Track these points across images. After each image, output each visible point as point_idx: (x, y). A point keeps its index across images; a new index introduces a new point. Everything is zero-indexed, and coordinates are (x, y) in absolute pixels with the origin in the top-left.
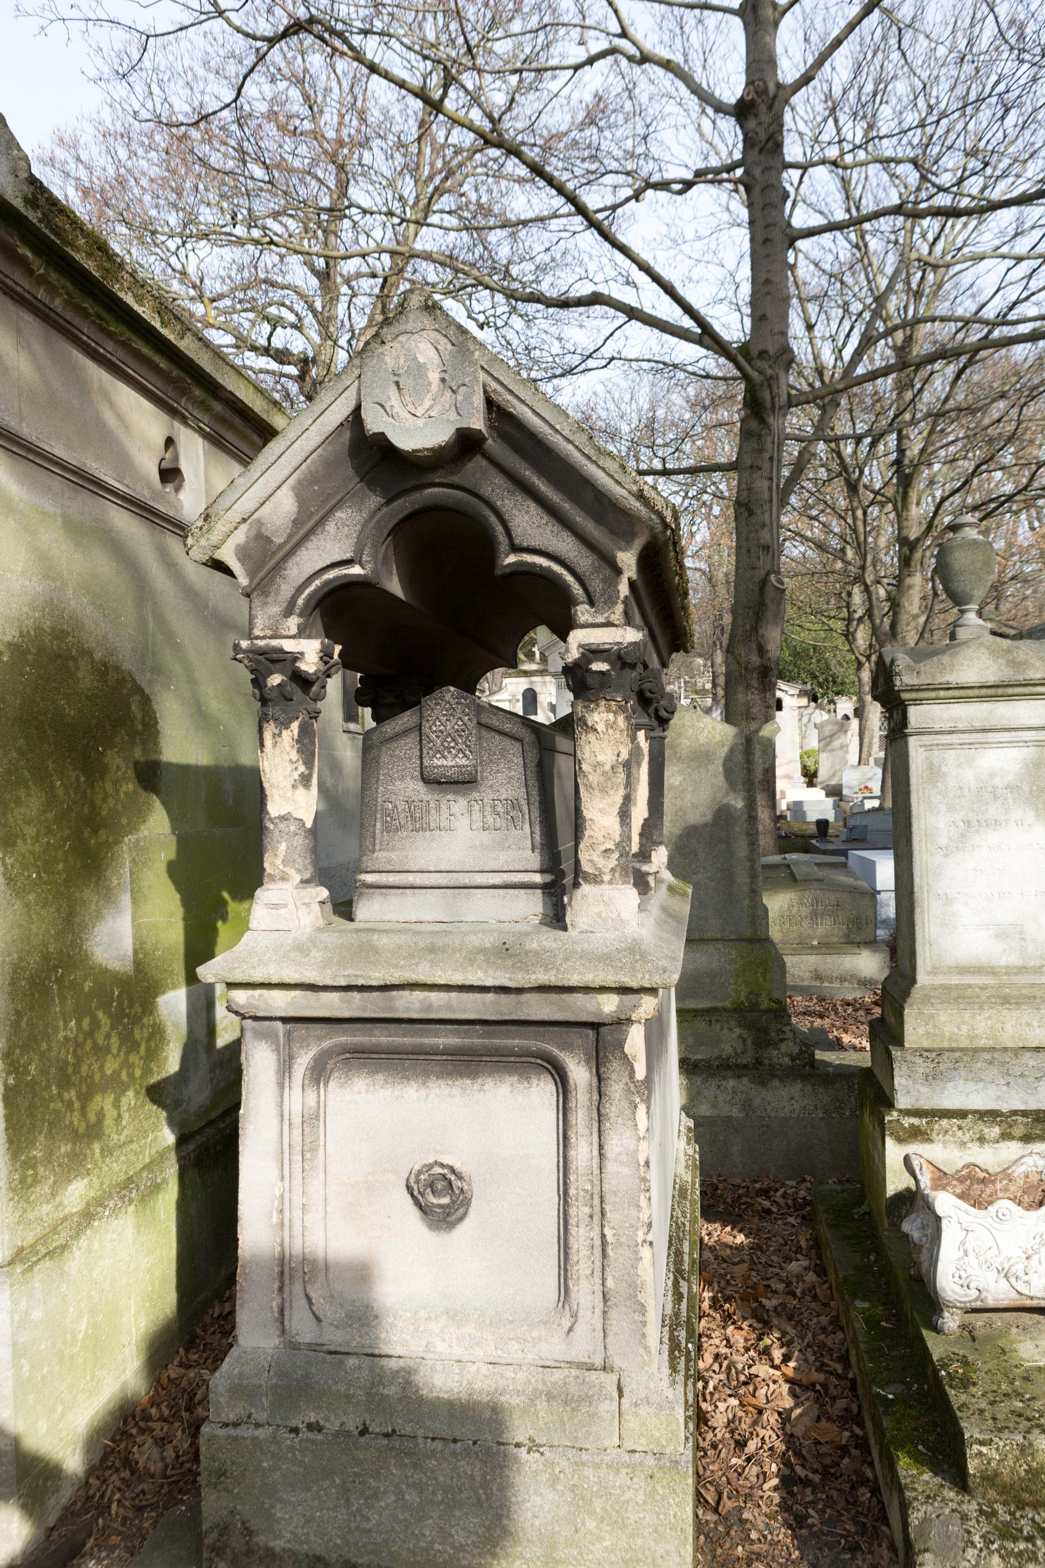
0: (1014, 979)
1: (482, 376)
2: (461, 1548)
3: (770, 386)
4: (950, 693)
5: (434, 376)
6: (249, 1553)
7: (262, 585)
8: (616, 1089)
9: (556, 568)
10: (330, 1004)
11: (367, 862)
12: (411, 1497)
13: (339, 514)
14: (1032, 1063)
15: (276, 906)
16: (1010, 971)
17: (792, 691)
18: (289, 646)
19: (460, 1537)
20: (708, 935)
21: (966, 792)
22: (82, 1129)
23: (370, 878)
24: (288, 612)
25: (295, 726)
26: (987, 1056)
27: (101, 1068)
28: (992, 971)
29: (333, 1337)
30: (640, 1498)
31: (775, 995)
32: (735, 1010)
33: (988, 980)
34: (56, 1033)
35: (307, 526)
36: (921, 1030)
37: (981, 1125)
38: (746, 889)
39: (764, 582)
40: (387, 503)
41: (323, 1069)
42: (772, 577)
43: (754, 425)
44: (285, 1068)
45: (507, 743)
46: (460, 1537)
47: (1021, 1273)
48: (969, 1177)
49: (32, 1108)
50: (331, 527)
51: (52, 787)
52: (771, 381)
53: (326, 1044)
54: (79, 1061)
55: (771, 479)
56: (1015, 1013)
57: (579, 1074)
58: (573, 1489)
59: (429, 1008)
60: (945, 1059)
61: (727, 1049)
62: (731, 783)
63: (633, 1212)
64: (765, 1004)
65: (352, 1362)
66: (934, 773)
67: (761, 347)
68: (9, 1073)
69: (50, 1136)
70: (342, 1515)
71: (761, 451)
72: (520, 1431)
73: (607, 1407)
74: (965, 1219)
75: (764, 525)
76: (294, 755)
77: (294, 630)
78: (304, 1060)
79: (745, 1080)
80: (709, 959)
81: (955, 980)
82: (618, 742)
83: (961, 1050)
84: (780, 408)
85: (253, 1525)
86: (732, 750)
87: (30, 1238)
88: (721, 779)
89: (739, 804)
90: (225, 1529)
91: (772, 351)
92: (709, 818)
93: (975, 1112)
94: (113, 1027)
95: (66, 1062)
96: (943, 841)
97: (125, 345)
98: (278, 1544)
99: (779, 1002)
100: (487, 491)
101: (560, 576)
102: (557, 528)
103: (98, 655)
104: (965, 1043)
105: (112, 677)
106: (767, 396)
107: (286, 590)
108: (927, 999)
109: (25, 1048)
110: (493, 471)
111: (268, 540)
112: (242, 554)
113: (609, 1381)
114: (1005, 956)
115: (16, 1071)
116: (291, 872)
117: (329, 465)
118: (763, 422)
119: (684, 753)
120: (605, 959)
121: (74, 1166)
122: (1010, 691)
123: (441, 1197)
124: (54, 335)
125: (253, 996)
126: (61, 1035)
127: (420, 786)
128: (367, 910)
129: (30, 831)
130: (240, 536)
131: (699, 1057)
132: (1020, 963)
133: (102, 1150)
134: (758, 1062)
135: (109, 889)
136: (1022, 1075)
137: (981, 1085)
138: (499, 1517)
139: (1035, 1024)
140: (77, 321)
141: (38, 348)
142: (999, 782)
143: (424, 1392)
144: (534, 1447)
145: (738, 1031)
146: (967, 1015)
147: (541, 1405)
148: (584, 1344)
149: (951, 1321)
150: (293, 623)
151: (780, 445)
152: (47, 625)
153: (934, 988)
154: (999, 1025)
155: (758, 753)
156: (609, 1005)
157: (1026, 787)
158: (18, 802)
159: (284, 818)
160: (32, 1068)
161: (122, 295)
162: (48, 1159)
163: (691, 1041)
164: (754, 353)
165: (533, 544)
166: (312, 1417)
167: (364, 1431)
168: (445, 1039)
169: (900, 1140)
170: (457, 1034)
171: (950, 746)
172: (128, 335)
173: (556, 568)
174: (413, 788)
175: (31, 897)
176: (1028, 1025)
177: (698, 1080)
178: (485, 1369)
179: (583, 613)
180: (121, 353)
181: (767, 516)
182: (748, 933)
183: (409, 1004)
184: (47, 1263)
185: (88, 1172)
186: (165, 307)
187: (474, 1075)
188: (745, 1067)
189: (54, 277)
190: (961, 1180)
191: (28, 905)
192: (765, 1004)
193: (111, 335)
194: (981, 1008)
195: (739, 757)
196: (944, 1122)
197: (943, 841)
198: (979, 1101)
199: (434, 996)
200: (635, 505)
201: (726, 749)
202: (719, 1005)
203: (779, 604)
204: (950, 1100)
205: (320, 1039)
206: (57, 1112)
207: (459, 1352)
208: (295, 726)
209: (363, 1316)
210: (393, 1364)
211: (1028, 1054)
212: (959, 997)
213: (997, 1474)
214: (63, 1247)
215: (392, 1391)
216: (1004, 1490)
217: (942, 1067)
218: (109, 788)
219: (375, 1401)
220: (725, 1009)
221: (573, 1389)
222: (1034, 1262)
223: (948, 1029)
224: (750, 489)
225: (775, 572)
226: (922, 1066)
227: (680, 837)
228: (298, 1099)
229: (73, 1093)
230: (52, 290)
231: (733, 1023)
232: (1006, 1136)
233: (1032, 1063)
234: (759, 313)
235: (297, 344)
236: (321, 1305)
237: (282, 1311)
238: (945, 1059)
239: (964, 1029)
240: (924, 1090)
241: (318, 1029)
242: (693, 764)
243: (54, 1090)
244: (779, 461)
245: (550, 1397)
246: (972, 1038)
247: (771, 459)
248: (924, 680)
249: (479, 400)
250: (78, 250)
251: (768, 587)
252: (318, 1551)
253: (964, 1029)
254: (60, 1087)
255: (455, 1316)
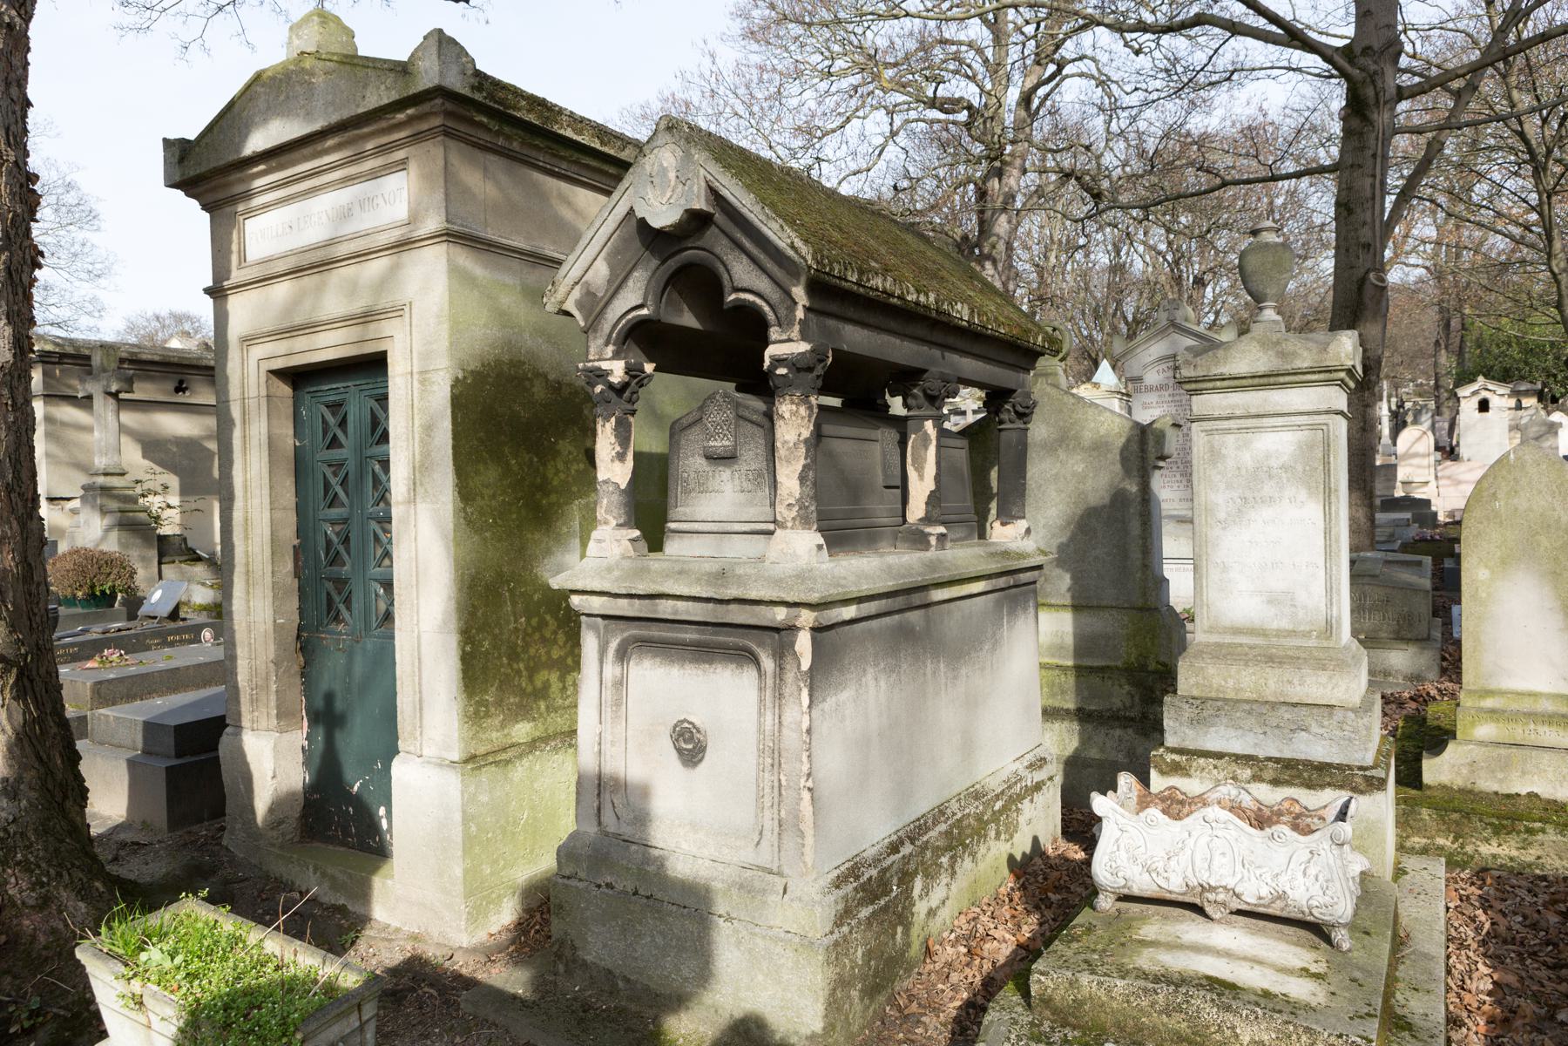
0: (1283, 641)
1: (702, 171)
2: (686, 979)
3: (1373, 82)
4: (1226, 383)
5: (672, 175)
6: (574, 961)
7: (591, 328)
8: (790, 676)
9: (759, 301)
10: (623, 607)
11: (672, 514)
12: (659, 940)
13: (636, 274)
14: (1287, 716)
15: (599, 541)
16: (1279, 633)
17: (1501, 391)
18: (605, 365)
19: (685, 972)
20: (1104, 603)
21: (1243, 472)
22: (529, 689)
23: (672, 526)
24: (607, 344)
25: (613, 420)
26: (1247, 707)
27: (548, 653)
28: (1263, 633)
29: (627, 831)
30: (790, 964)
31: (1162, 659)
32: (1126, 670)
33: (1259, 641)
34: (508, 623)
35: (617, 286)
36: (1192, 681)
37: (1234, 767)
38: (1138, 563)
39: (1363, 281)
40: (663, 262)
41: (625, 652)
42: (1372, 276)
43: (1355, 123)
44: (602, 652)
45: (756, 430)
46: (685, 972)
47: (1161, 870)
48: (1170, 798)
49: (485, 669)
50: (630, 283)
51: (508, 463)
52: (1373, 78)
53: (626, 634)
54: (527, 646)
55: (1374, 176)
56: (1278, 671)
57: (768, 664)
58: (750, 951)
59: (676, 612)
60: (1211, 707)
61: (1117, 703)
62: (1127, 471)
63: (798, 765)
64: (1152, 666)
65: (634, 847)
66: (1215, 455)
67: (1366, 43)
68: (466, 644)
69: (500, 688)
70: (622, 945)
71: (1363, 149)
72: (721, 907)
73: (774, 898)
74: (1121, 820)
75: (1365, 223)
76: (613, 440)
77: (610, 355)
78: (614, 645)
79: (1130, 731)
80: (1098, 623)
81: (1228, 639)
82: (799, 426)
83: (1225, 700)
84: (1385, 103)
85: (578, 943)
86: (1128, 441)
87: (482, 750)
88: (1119, 466)
89: (1133, 488)
90: (562, 943)
91: (1376, 46)
92: (1107, 501)
93: (1230, 755)
94: (559, 627)
95: (516, 645)
96: (1222, 515)
97: (576, 163)
98: (589, 958)
99: (1164, 665)
100: (718, 250)
101: (760, 307)
102: (759, 272)
103: (552, 377)
104: (1231, 695)
105: (565, 391)
106: (1370, 92)
107: (607, 327)
108: (1200, 654)
109: (479, 630)
110: (722, 236)
111: (594, 295)
112: (580, 305)
113: (779, 883)
114: (1277, 621)
115: (473, 644)
116: (610, 518)
117: (625, 241)
118: (1365, 119)
119: (1086, 444)
120: (778, 582)
121: (522, 712)
122: (1282, 379)
123: (690, 746)
124: (516, 166)
125: (1501, 781)
126: (512, 626)
127: (703, 461)
128: (673, 547)
129: (488, 492)
130: (577, 293)
131: (1093, 708)
132: (1291, 627)
133: (547, 708)
134: (1144, 716)
135: (559, 534)
136: (1278, 727)
137: (1240, 732)
138: (708, 963)
139: (1296, 682)
140: (534, 154)
141: (503, 178)
142: (1274, 463)
143: (669, 873)
144: (729, 919)
145: (1127, 687)
146: (1234, 669)
147: (734, 891)
148: (765, 857)
149: (1105, 902)
150: (610, 350)
151: (1386, 142)
152: (506, 358)
153: (1208, 645)
154: (1262, 681)
155: (1151, 443)
156: (781, 614)
157: (1300, 468)
158: (477, 473)
159: (606, 482)
160: (486, 644)
161: (561, 132)
162: (499, 703)
163: (1086, 693)
164: (1358, 50)
165: (745, 285)
166: (609, 879)
167: (636, 893)
168: (690, 635)
169: (1162, 773)
170: (698, 632)
171: (1228, 431)
172: (576, 156)
173: (759, 301)
174: (699, 462)
175: (488, 534)
176: (1290, 682)
177: (1090, 727)
178: (708, 863)
179: (774, 333)
180: (575, 168)
181: (1369, 214)
182: (1140, 603)
183: (665, 609)
184: (493, 768)
185: (534, 719)
186: (602, 132)
187: (710, 662)
188: (1132, 719)
189: (507, 129)
190: (1163, 800)
191: (485, 539)
192: (1152, 666)
193: (563, 158)
194: (1246, 665)
195: (1135, 447)
196: (1202, 761)
197: (1222, 515)
198: (1238, 746)
199: (680, 604)
200: (791, 253)
201: (1123, 440)
202: (1109, 663)
203: (1379, 302)
204: (1213, 742)
205: (623, 631)
206: (507, 675)
207: (694, 851)
208: (613, 420)
209: (642, 819)
210: (656, 853)
211: (1284, 708)
212: (1223, 654)
213: (1051, 999)
214: (508, 762)
215: (651, 869)
216: (1055, 1011)
217: (1205, 714)
218: (561, 466)
219: (642, 875)
220: (1117, 668)
221: (757, 884)
222: (1173, 863)
223: (1217, 681)
224: (1349, 189)
225: (1375, 269)
226: (1188, 712)
227: (1082, 517)
228: (611, 670)
229: (521, 666)
230: (508, 138)
231: (1123, 681)
232: (1256, 778)
233: (1287, 716)
234: (1363, 10)
235: (970, 92)
236: (620, 809)
237: (599, 809)
238: (1211, 707)
239: (1231, 683)
240: (1190, 733)
241: (622, 624)
242: (1095, 454)
243: (505, 660)
244: (1385, 157)
245: (741, 887)
246: (1237, 691)
247: (1374, 156)
248: (1200, 372)
249: (703, 184)
250: (519, 110)
251: (1367, 287)
252: (610, 966)
253: (1231, 683)
254: (510, 659)
255: (694, 826)
